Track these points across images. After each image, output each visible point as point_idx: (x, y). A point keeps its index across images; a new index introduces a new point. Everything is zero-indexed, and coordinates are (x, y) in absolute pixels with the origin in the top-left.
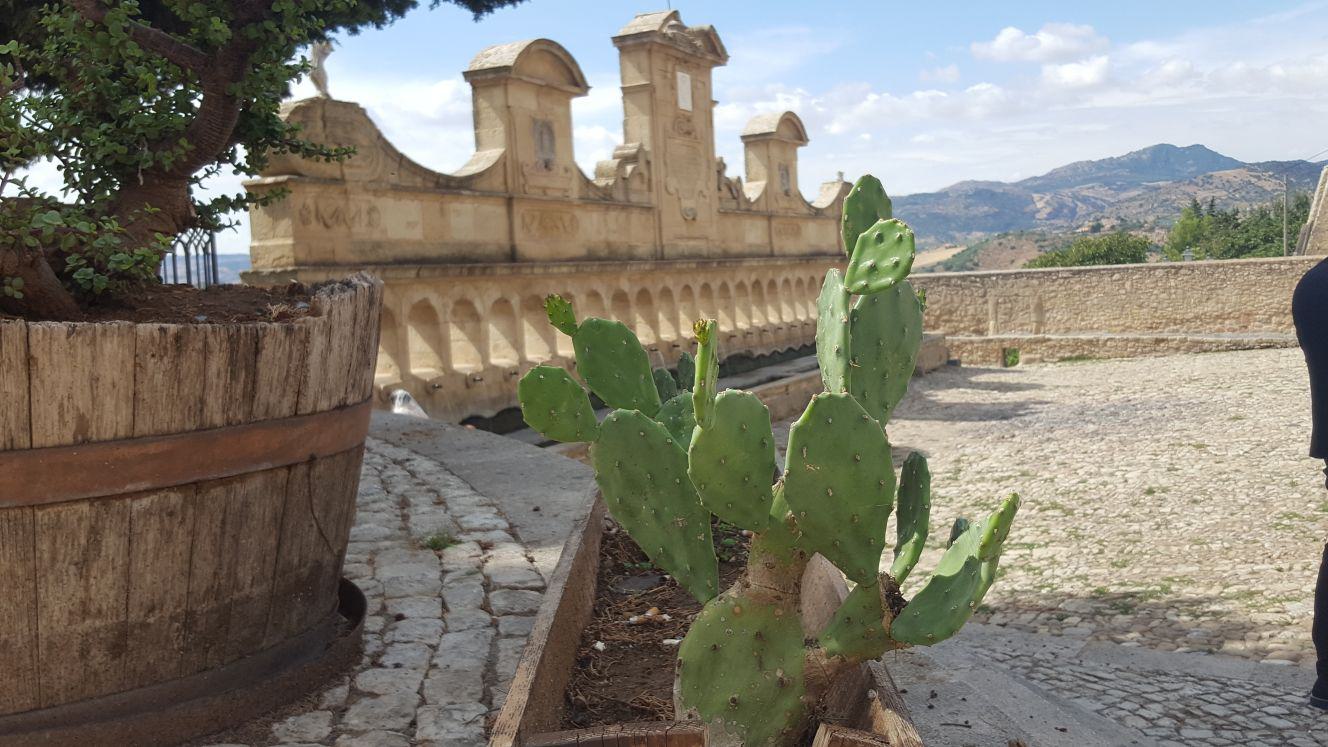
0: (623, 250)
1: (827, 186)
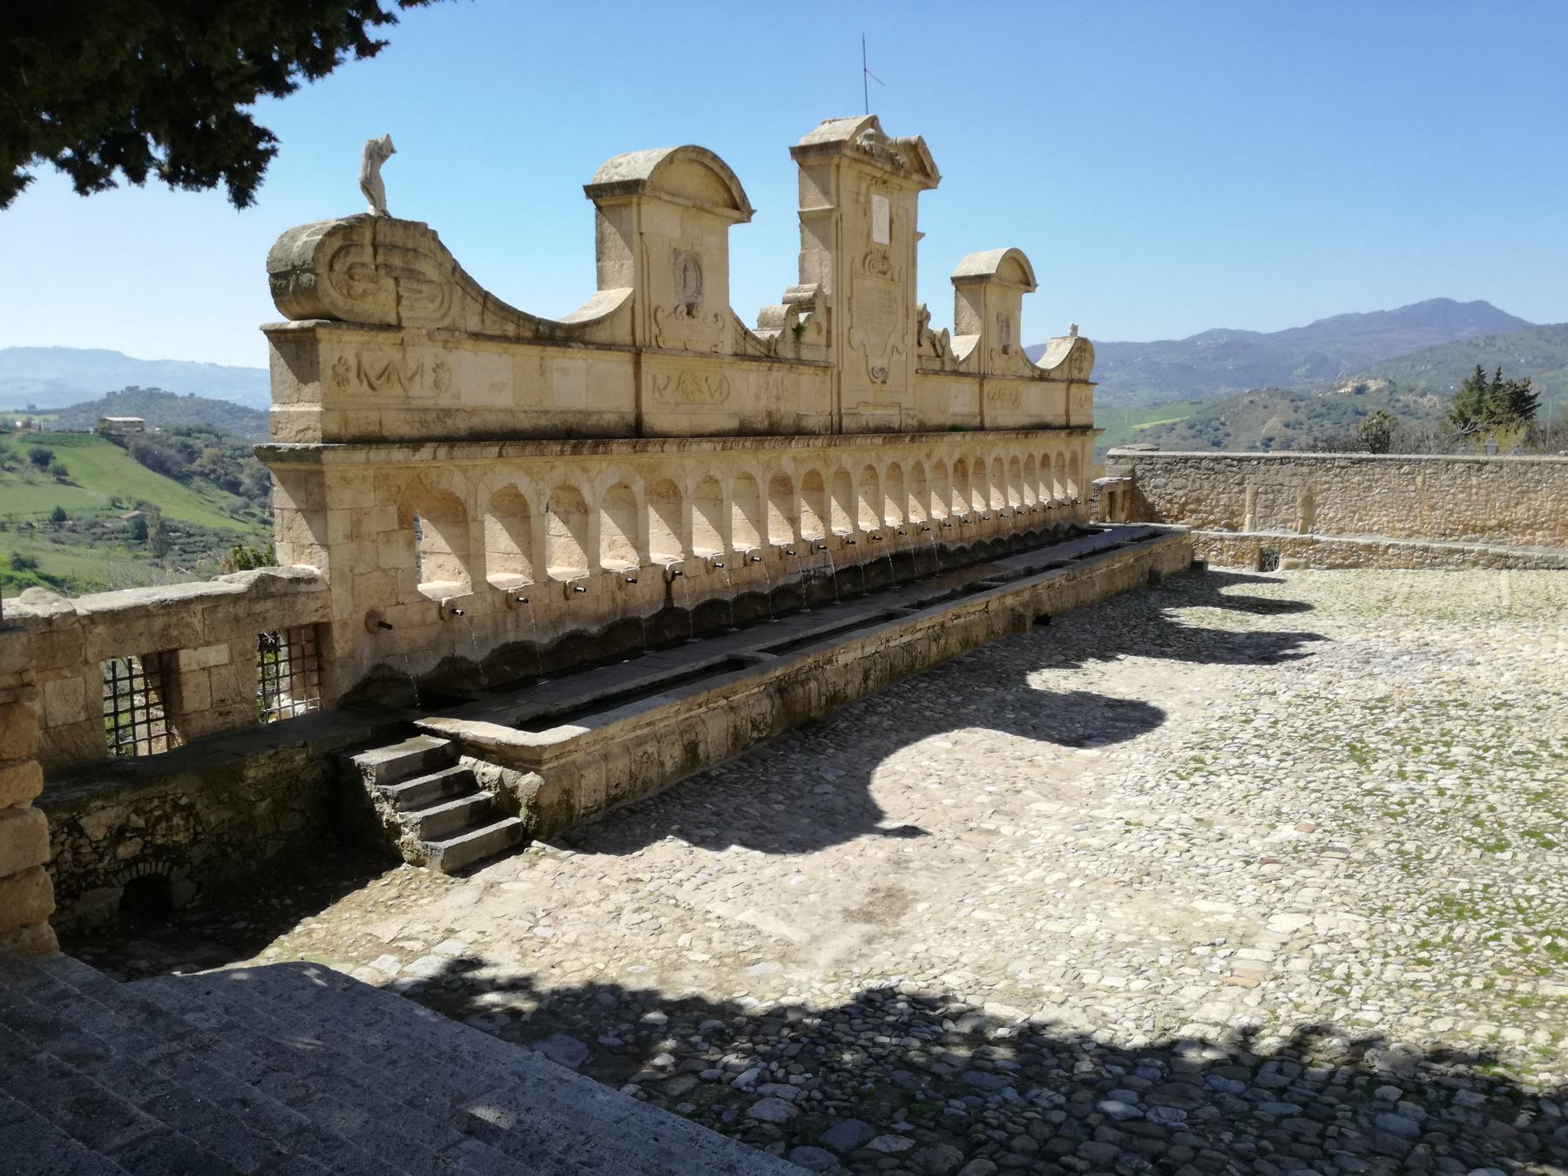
0: (788, 421)
1: (1055, 341)
